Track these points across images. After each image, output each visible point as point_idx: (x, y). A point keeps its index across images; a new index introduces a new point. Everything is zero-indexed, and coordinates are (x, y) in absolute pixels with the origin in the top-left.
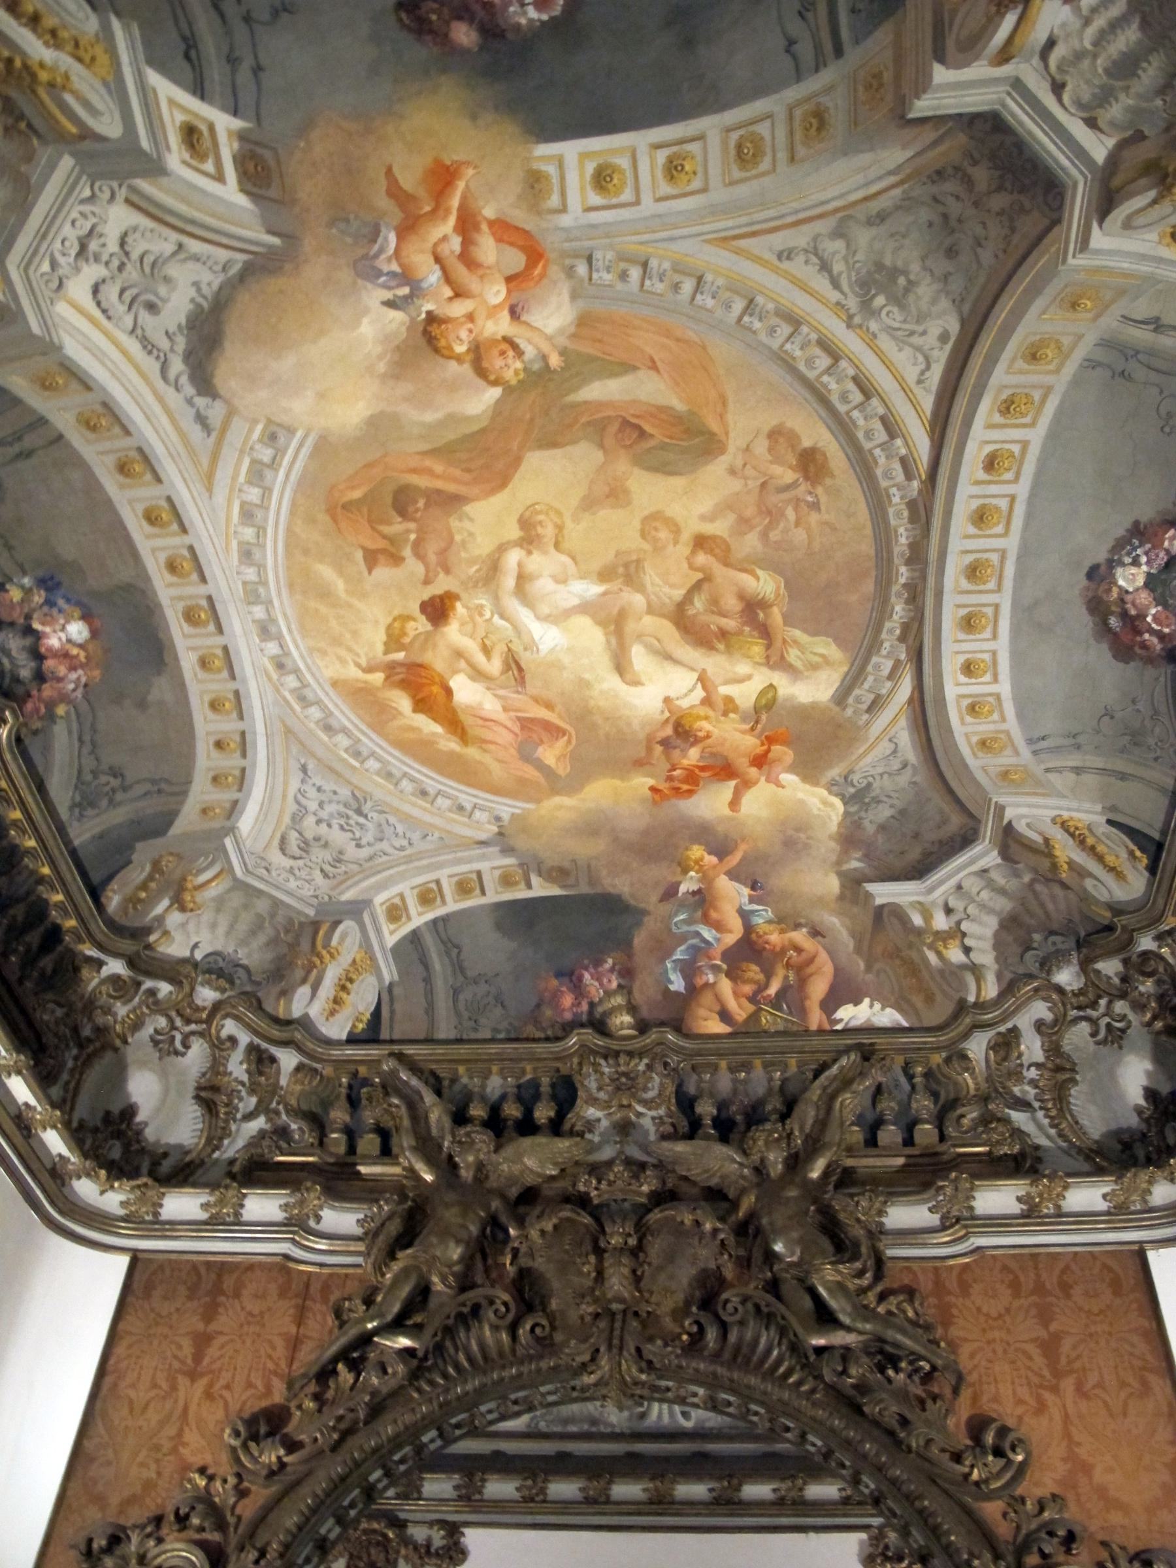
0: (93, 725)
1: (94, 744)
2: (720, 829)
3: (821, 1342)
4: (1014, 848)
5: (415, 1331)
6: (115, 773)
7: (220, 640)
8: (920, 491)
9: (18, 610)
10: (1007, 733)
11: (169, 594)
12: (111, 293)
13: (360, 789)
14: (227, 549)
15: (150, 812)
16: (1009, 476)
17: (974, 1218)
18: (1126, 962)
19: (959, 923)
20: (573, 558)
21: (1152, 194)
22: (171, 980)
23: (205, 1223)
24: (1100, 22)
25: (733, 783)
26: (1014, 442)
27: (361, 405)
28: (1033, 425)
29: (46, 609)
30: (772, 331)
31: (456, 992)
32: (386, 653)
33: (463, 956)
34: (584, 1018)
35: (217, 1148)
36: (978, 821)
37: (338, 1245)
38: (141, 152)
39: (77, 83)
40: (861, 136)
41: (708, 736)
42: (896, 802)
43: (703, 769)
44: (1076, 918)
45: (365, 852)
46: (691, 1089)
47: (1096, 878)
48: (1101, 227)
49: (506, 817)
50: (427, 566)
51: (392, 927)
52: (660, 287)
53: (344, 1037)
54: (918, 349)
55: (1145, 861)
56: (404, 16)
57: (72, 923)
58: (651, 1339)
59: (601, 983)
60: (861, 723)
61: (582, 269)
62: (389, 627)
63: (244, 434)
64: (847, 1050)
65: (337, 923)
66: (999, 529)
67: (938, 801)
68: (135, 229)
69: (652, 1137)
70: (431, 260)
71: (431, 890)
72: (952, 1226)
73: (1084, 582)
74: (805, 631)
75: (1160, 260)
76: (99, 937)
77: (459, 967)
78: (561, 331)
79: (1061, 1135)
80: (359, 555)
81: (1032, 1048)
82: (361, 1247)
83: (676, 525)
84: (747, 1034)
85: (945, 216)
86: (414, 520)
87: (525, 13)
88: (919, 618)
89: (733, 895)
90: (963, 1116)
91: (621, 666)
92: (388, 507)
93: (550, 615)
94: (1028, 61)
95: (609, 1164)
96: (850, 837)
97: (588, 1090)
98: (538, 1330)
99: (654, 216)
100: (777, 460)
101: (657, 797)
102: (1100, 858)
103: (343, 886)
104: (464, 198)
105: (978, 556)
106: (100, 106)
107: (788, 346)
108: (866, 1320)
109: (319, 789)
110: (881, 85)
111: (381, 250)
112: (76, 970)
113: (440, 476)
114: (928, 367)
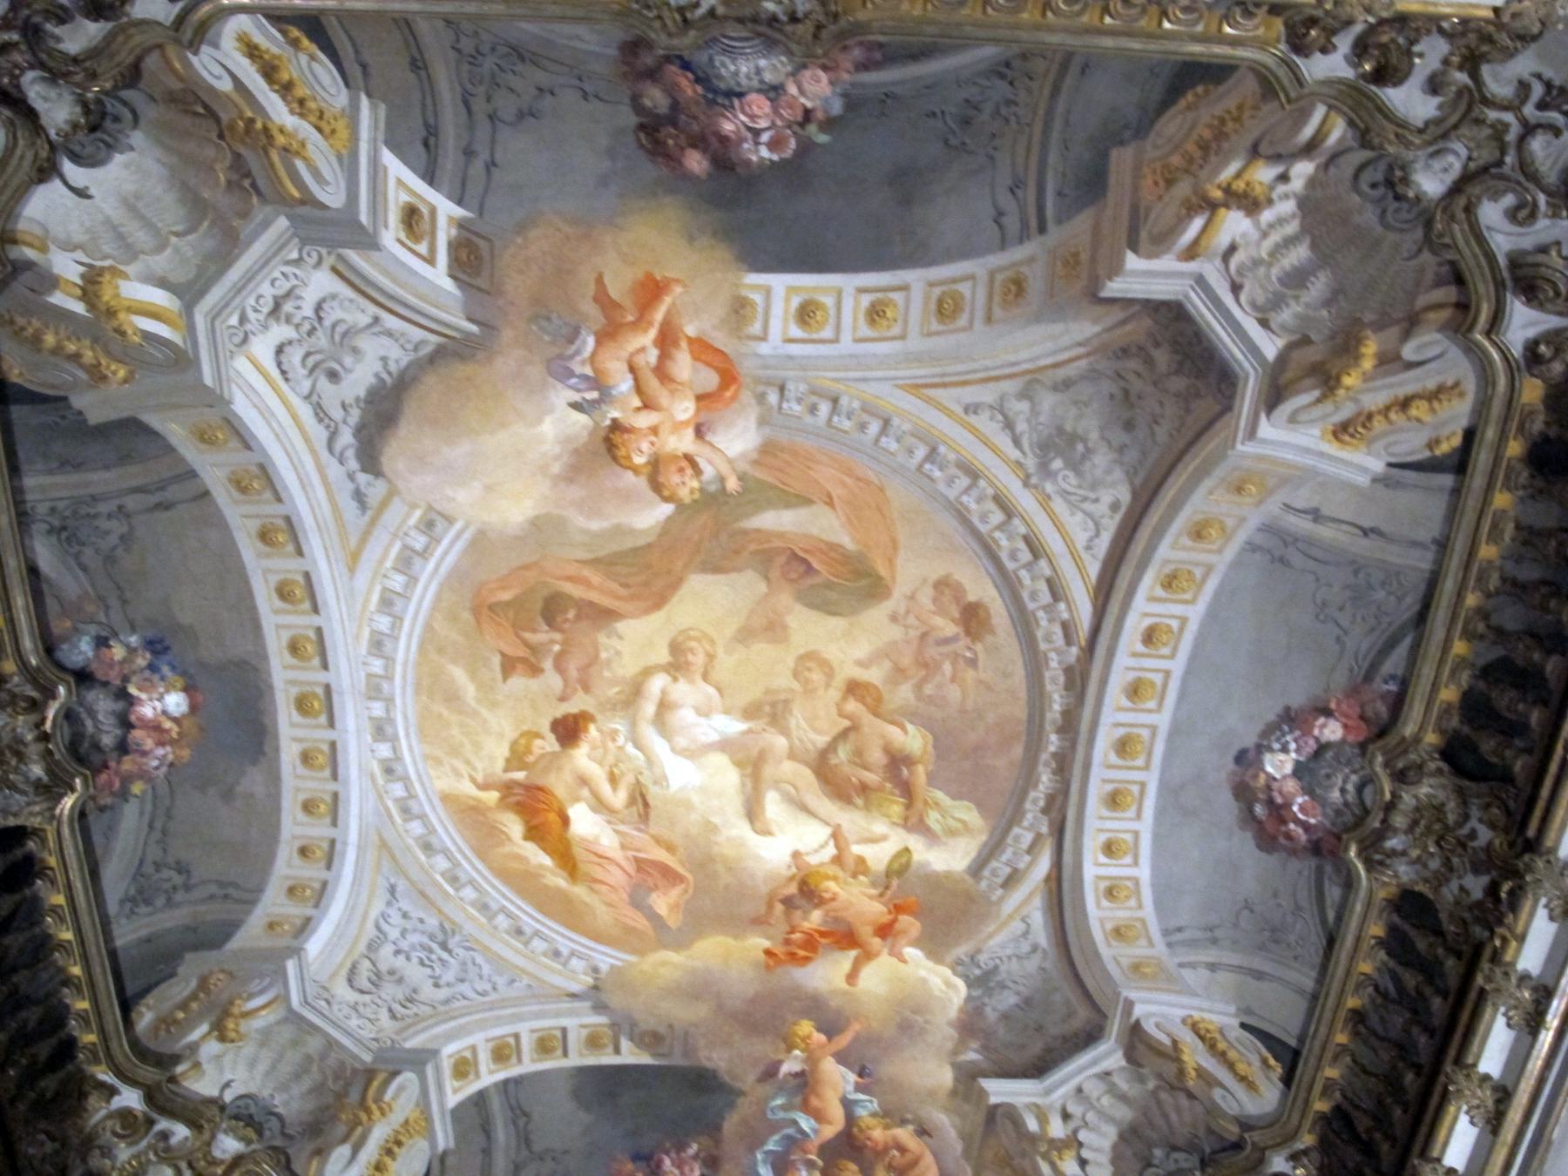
0: (169, 809)
1: (164, 832)
2: (833, 1003)
4: (1141, 1047)
6: (181, 868)
7: (330, 735)
8: (1078, 660)
9: (117, 668)
10: (1143, 921)
11: (284, 676)
12: (295, 356)
13: (448, 919)
14: (357, 637)
15: (207, 926)
16: (1165, 651)
19: (1075, 1132)
20: (719, 690)
21: (1316, 393)
24: (1275, 237)
25: (853, 953)
26: (1174, 617)
29: (147, 673)
30: (950, 482)
32: (506, 770)
33: (530, 1127)
36: (1105, 1016)
38: (361, 226)
39: (311, 151)
40: (1054, 308)
41: (833, 899)
42: (1021, 988)
43: (823, 934)
44: (1201, 1133)
45: (443, 993)
49: (604, 968)
50: (565, 681)
51: (456, 1084)
52: (847, 425)
55: (1280, 1070)
56: (642, 135)
57: (91, 1038)
60: (994, 898)
61: (773, 398)
62: (514, 745)
63: (402, 517)
65: (395, 1074)
66: (1152, 704)
67: (1068, 992)
68: (334, 297)
70: (625, 367)
71: (508, 1045)
73: (1231, 766)
74: (948, 793)
75: (1322, 454)
76: (119, 1058)
78: (743, 455)
80: (496, 660)
83: (831, 668)
85: (1126, 393)
87: (757, 151)
88: (1065, 791)
89: (838, 1079)
91: (753, 812)
92: (537, 613)
93: (686, 750)
94: (1210, 261)
96: (970, 1025)
99: (851, 356)
100: (941, 611)
101: (771, 962)
102: (1231, 1066)
103: (411, 1031)
104: (668, 313)
105: (1128, 730)
107: (965, 499)
109: (405, 915)
110: (1077, 263)
111: (578, 352)
112: (83, 1096)
114: (1097, 534)
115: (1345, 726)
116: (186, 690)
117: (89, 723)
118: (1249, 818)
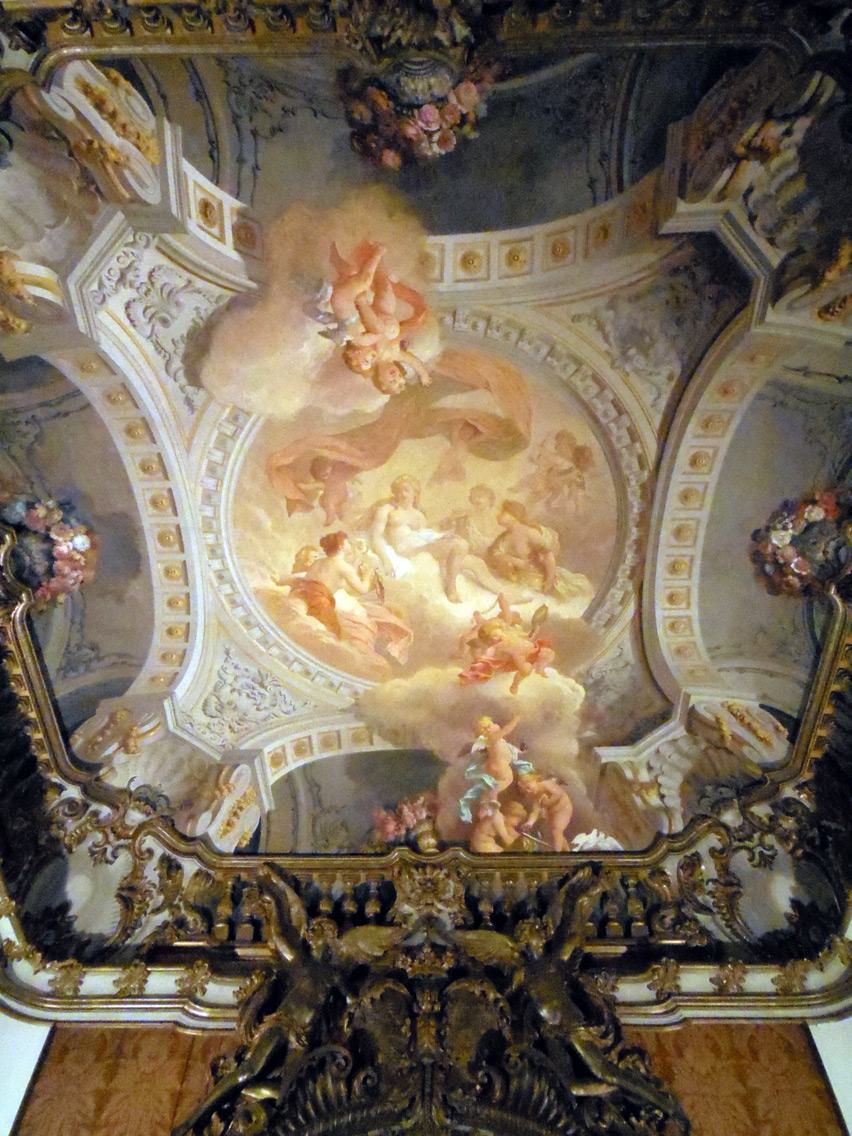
3: (582, 1092)
4: (696, 725)
5: (274, 1084)
8: (649, 479)
11: (150, 521)
13: (264, 668)
15: (112, 686)
16: (705, 469)
17: (680, 994)
18: (774, 806)
19: (656, 777)
22: (113, 806)
23: (115, 997)
24: (782, 177)
25: (513, 674)
27: (297, 400)
28: (723, 436)
30: (565, 367)
31: (315, 819)
34: (402, 840)
35: (129, 936)
36: (672, 705)
37: (217, 1013)
41: (500, 640)
45: (263, 714)
46: (475, 893)
47: (750, 746)
48: (773, 306)
49: (361, 691)
51: (274, 770)
53: (232, 851)
54: (653, 384)
55: (787, 733)
58: (453, 1089)
59: (414, 815)
61: (448, 320)
64: (582, 866)
65: (236, 766)
67: (649, 690)
68: (160, 267)
69: (449, 927)
70: (353, 305)
71: (303, 744)
72: (663, 1001)
75: (812, 330)
77: (318, 802)
79: (734, 931)
80: (283, 503)
81: (708, 869)
82: (235, 1014)
84: (514, 854)
85: (677, 298)
86: (324, 481)
87: (431, 148)
88: (643, 562)
89: (507, 752)
90: (664, 917)
91: (448, 589)
92: (308, 470)
95: (420, 947)
96: (588, 715)
97: (404, 892)
98: (369, 1081)
104: (378, 268)
106: (148, 182)
108: (613, 1075)
109: (236, 667)
111: (322, 298)
112: (44, 792)
113: (341, 453)
114: (659, 396)
115: (826, 511)
116: (87, 533)
117: (27, 559)
118: (761, 573)
